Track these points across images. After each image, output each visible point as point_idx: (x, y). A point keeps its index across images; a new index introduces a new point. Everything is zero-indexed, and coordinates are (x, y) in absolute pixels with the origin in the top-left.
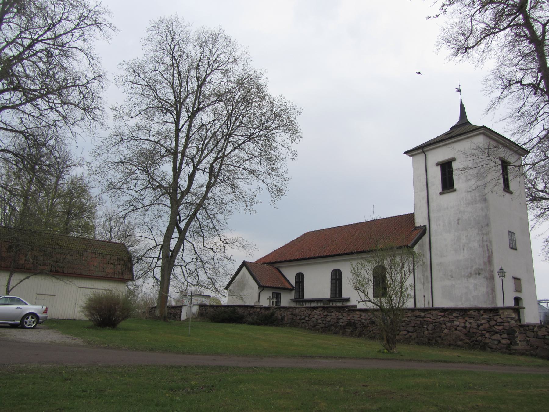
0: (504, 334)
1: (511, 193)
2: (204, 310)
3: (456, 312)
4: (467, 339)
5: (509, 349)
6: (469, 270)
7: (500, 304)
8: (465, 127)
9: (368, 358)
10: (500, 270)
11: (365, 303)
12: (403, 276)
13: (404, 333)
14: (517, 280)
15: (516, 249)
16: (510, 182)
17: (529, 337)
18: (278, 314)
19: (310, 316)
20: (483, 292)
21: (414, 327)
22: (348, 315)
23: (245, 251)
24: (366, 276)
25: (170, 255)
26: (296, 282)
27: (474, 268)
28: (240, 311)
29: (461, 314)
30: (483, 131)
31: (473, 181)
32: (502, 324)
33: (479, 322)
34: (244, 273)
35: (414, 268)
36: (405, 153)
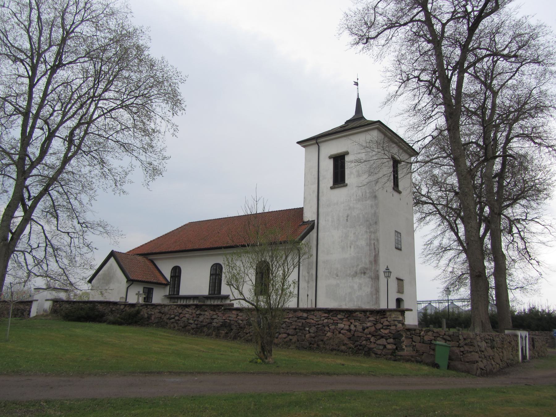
0: (390, 338)
1: (400, 192)
2: (58, 306)
3: (341, 313)
4: (350, 343)
5: (394, 354)
6: (355, 269)
7: (383, 306)
8: (360, 122)
10: (386, 269)
11: (239, 302)
12: (286, 270)
14: (400, 280)
15: (400, 250)
16: (399, 180)
17: (415, 342)
18: (144, 312)
19: (181, 315)
21: (295, 329)
24: (242, 268)
25: (9, 238)
26: (171, 277)
27: (359, 267)
28: (101, 307)
29: (346, 316)
30: (378, 126)
31: (366, 176)
32: (389, 327)
33: (365, 325)
34: (111, 265)
35: (299, 262)
36: (298, 143)
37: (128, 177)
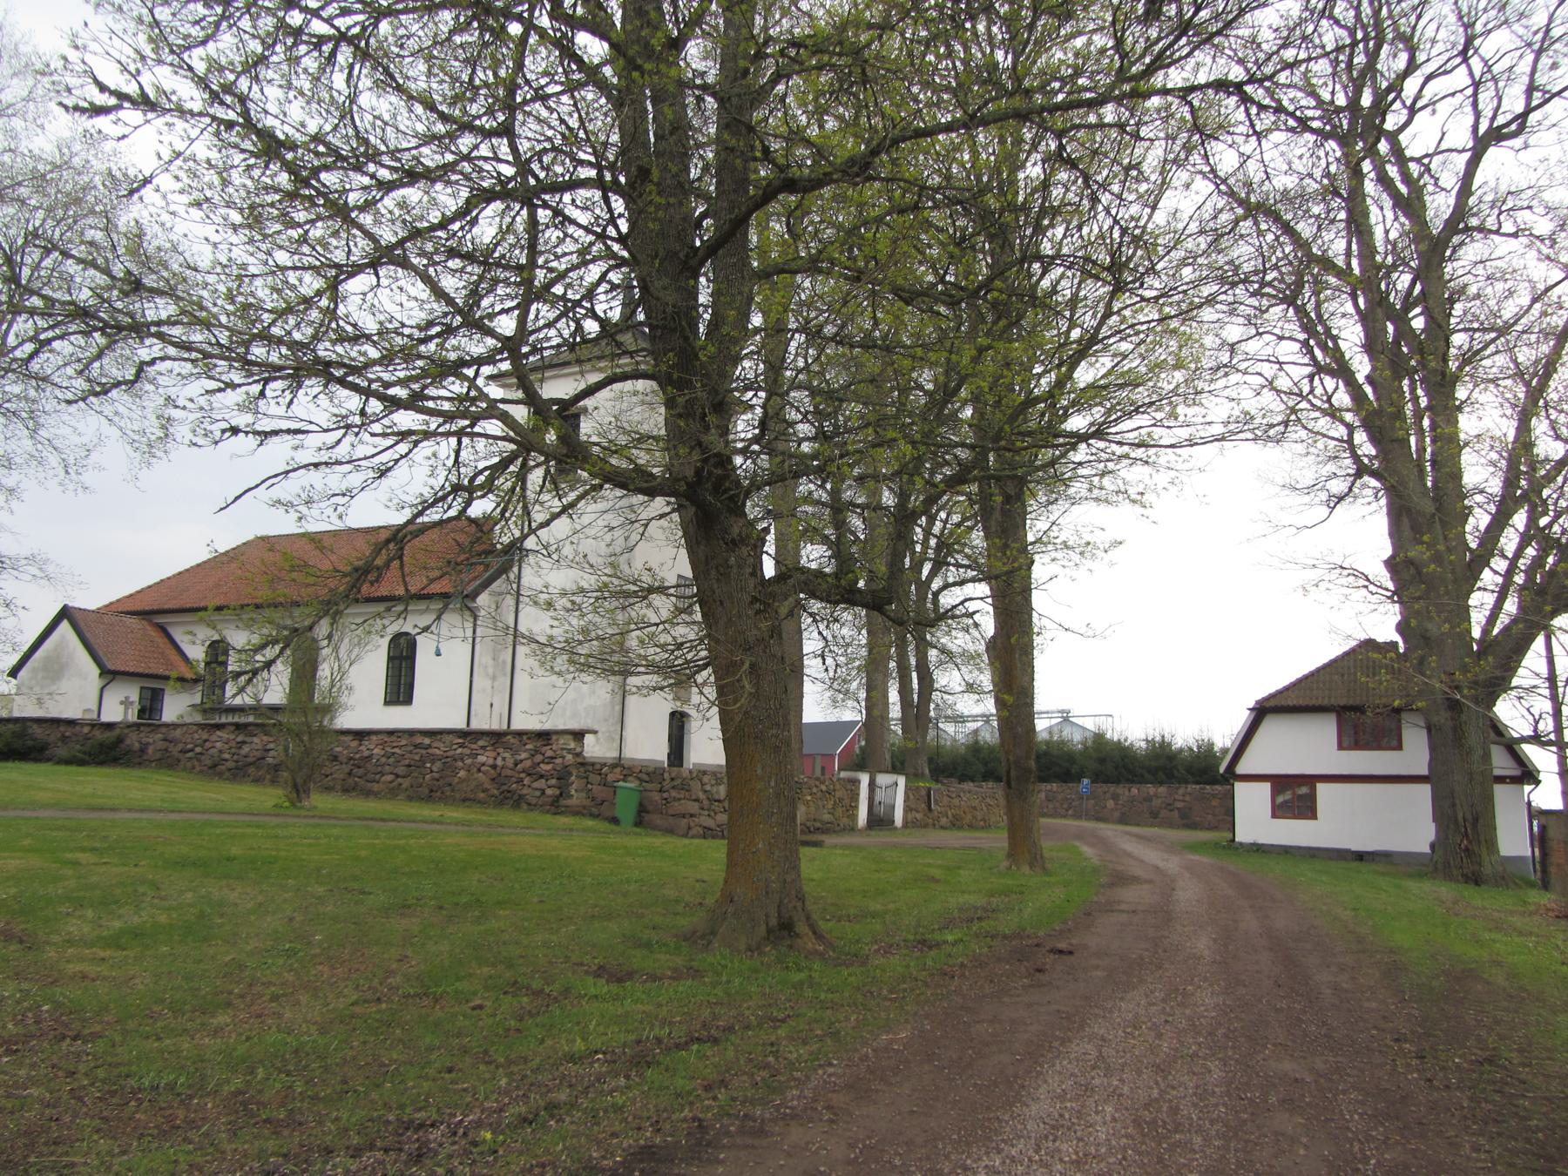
13: (390, 777)
18: (133, 741)
34: (63, 637)
37: (94, 456)
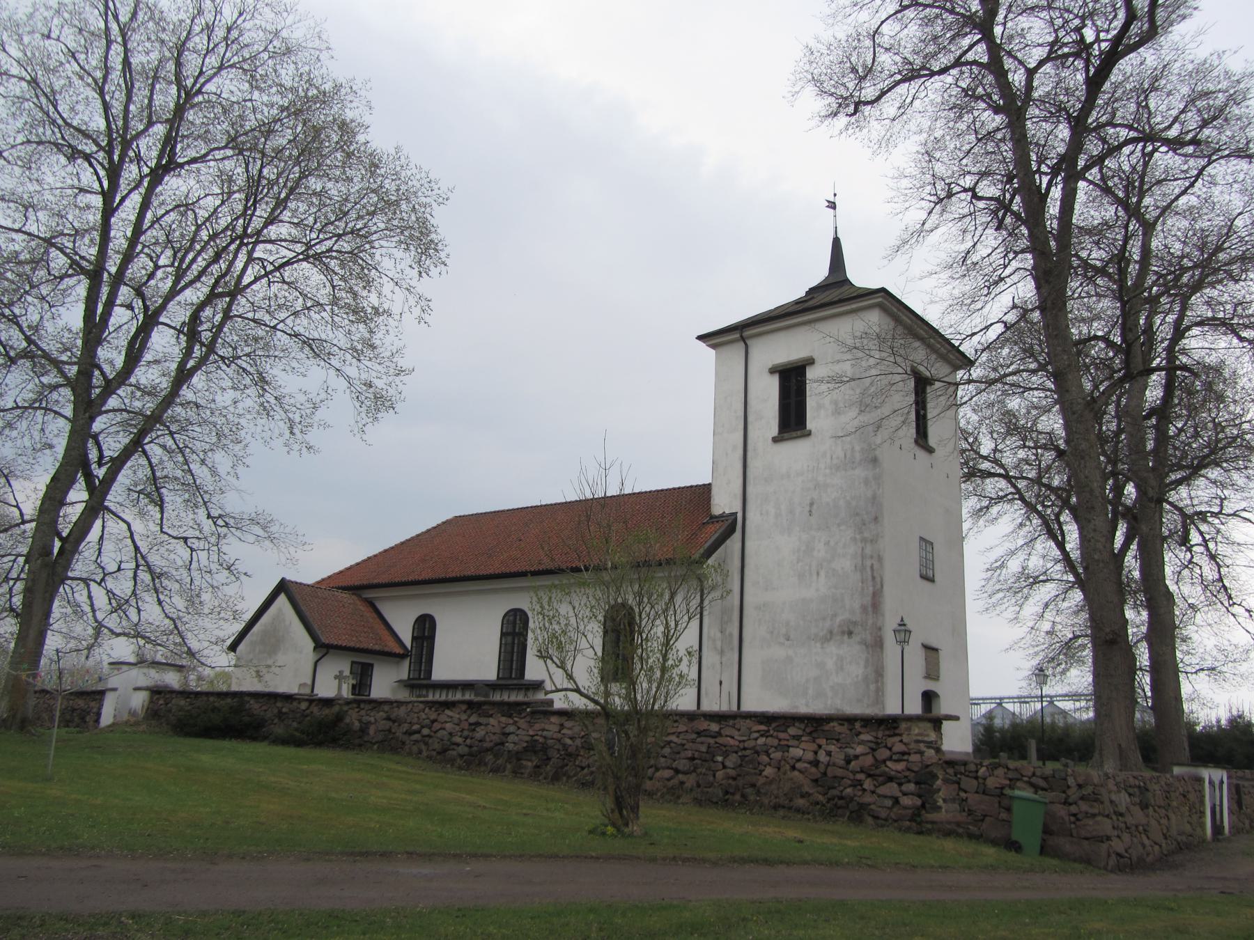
0: (909, 781)
1: (930, 450)
2: (161, 702)
3: (797, 724)
5: (918, 819)
6: (828, 624)
7: (892, 708)
9: (555, 857)
10: (900, 625)
11: (566, 697)
12: (672, 624)
13: (667, 773)
14: (931, 650)
16: (929, 423)
17: (966, 792)
18: (353, 719)
19: (435, 724)
20: (857, 676)
21: (693, 759)
22: (531, 724)
23: (275, 551)
24: (573, 620)
25: (56, 551)
26: (414, 638)
27: (838, 620)
29: (808, 730)
30: (880, 300)
31: (853, 413)
32: (906, 757)
33: (851, 752)
34: (280, 610)
36: (700, 338)
37: (320, 414)
